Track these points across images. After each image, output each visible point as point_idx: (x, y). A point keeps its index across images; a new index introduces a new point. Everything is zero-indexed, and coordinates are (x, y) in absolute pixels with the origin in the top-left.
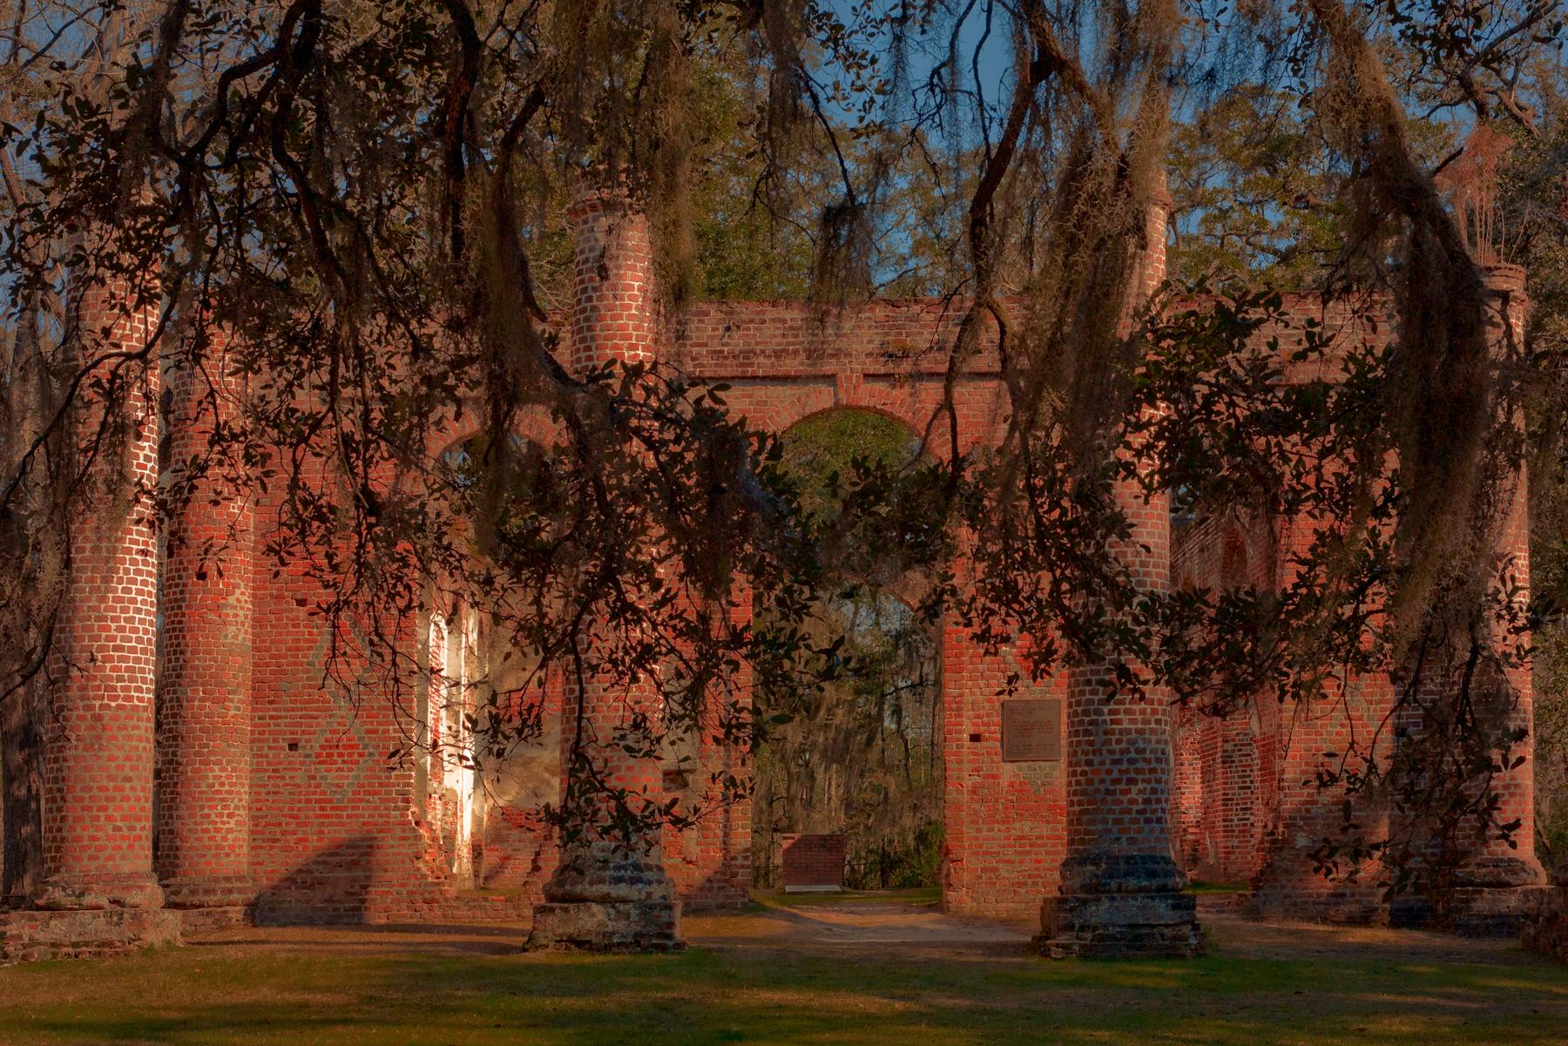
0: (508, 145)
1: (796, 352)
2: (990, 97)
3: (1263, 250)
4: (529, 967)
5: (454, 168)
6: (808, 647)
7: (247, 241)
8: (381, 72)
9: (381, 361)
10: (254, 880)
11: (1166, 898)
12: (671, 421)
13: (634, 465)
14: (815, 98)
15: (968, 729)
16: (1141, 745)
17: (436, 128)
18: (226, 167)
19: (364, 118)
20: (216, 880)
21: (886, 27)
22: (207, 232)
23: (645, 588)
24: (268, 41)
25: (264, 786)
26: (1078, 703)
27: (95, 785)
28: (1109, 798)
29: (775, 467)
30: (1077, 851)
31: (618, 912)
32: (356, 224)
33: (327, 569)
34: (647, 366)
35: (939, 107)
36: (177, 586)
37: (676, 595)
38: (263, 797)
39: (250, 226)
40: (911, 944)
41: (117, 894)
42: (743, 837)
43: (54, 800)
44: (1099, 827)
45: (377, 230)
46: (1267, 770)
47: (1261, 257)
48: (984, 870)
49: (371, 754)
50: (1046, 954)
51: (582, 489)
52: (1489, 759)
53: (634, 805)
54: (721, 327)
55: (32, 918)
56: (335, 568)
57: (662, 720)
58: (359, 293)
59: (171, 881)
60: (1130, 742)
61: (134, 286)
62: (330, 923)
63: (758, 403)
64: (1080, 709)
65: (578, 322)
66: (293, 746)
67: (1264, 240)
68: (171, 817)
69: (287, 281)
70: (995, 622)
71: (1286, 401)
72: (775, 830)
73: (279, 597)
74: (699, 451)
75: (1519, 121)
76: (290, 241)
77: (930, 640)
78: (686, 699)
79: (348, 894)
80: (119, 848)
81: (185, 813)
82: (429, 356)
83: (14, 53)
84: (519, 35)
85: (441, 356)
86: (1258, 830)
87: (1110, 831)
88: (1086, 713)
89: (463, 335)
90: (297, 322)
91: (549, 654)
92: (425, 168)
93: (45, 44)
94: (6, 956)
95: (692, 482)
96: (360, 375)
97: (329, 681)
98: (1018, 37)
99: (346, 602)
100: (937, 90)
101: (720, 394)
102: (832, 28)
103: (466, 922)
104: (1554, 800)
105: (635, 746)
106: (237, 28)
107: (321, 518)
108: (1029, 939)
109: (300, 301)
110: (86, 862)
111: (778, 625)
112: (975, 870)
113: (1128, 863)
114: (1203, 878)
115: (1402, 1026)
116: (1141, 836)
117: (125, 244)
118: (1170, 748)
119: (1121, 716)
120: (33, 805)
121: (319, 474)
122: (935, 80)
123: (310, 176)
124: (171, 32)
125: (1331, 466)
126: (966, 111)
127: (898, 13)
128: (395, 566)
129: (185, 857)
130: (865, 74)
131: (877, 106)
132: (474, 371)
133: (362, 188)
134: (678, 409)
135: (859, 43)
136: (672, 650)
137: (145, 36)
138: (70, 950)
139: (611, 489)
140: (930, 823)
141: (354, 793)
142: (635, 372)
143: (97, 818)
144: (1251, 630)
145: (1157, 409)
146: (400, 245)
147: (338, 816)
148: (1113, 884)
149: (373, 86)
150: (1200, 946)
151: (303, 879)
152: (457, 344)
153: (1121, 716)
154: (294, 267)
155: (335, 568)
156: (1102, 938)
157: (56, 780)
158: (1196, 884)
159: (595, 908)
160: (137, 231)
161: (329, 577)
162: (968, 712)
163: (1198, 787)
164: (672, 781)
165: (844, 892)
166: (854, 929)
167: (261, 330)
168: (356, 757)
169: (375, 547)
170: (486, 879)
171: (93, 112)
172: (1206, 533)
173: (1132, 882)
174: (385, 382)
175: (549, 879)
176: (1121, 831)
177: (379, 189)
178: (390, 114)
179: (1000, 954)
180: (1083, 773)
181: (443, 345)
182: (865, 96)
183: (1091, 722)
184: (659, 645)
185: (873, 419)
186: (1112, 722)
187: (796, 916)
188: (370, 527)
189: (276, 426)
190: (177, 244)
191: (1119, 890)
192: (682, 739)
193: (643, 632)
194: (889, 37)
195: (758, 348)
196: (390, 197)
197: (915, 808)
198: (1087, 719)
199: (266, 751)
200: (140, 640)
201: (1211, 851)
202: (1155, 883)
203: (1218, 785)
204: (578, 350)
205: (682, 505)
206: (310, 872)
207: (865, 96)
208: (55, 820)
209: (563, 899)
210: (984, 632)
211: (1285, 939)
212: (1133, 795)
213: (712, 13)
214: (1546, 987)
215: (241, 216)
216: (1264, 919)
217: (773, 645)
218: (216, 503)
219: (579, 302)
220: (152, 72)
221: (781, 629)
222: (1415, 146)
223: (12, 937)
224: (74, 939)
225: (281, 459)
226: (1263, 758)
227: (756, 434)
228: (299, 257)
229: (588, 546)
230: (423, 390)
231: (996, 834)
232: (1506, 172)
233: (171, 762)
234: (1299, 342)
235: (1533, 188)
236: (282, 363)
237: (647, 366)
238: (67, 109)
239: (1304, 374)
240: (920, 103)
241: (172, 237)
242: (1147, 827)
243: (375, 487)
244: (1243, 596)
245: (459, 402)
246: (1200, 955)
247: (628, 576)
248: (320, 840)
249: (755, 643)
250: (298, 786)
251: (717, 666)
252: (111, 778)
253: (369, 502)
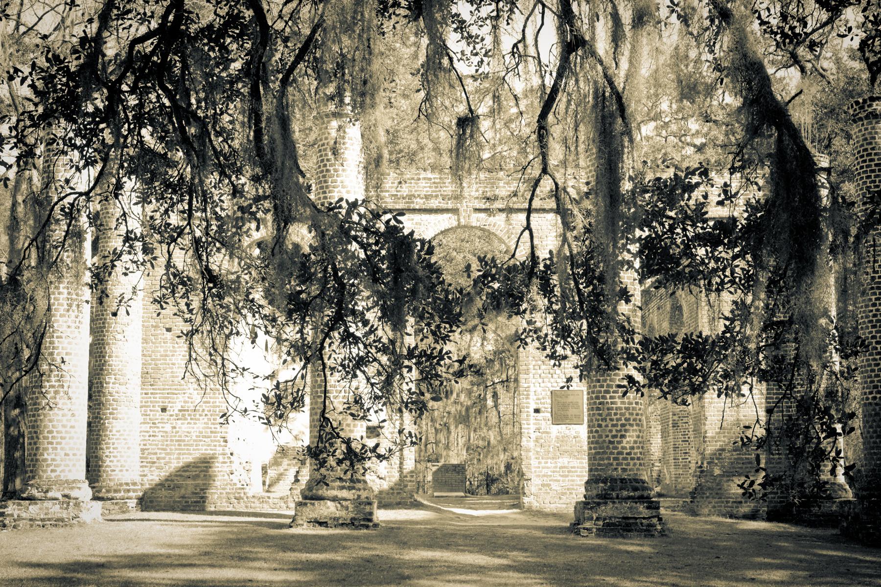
0: (285, 82)
1: (437, 196)
2: (544, 60)
3: (688, 144)
4: (293, 536)
5: (255, 94)
6: (449, 358)
7: (144, 132)
8: (216, 41)
9: (216, 198)
10: (142, 485)
11: (644, 503)
12: (373, 233)
13: (354, 256)
14: (451, 59)
15: (533, 406)
16: (627, 416)
17: (246, 71)
18: (132, 91)
19: (207, 66)
20: (121, 485)
21: (488, 22)
22: (123, 126)
23: (360, 324)
24: (154, 25)
25: (147, 432)
26: (593, 392)
27: (55, 430)
28: (611, 446)
29: (430, 258)
30: (594, 475)
31: (342, 506)
32: (202, 123)
33: (186, 311)
34: (360, 203)
35: (517, 64)
36: (101, 319)
37: (376, 329)
38: (147, 438)
39: (146, 124)
40: (504, 527)
41: (66, 492)
42: (409, 465)
43: (32, 438)
44: (606, 462)
45: (214, 127)
46: (697, 431)
47: (687, 148)
50: (578, 533)
51: (325, 270)
52: (835, 429)
53: (356, 446)
54: (396, 182)
55: (19, 505)
56: (191, 311)
57: (371, 398)
58: (204, 161)
59: (96, 485)
60: (622, 414)
61: (83, 156)
62: (184, 510)
64: (594, 396)
65: (319, 178)
66: (164, 410)
67: (688, 139)
68: (96, 448)
69: (166, 154)
70: (558, 348)
71: (714, 228)
72: (429, 461)
73: (156, 327)
74: (388, 248)
75: (823, 76)
76: (167, 132)
77: (512, 356)
78: (383, 387)
79: (194, 493)
80: (68, 465)
81: (104, 447)
82: (242, 196)
83: (17, 28)
84: (290, 23)
85: (249, 196)
86: (693, 466)
87: (612, 464)
88: (597, 398)
89: (260, 184)
90: (171, 176)
91: (308, 360)
92: (238, 93)
93: (33, 23)
94: (4, 526)
95: (384, 267)
96: (205, 206)
97: (187, 374)
98: (561, 30)
99: (197, 331)
100: (516, 55)
101: (399, 218)
102: (459, 22)
103: (258, 510)
104: (855, 450)
105: (356, 413)
106: (139, 17)
107: (184, 284)
108: (568, 525)
109: (173, 164)
110: (49, 473)
111: (432, 345)
112: (538, 485)
113: (622, 482)
114: (663, 492)
115: (778, 575)
116: (629, 467)
117: (78, 132)
118: (644, 418)
120: (21, 440)
121: (182, 259)
122: (515, 50)
123: (178, 97)
124: (104, 18)
125: (740, 263)
126: (532, 65)
127: (494, 14)
128: (224, 311)
129: (104, 471)
130: (478, 47)
131: (485, 63)
132: (267, 204)
133: (206, 103)
134: (377, 226)
135: (474, 30)
136: (375, 360)
137: (90, 21)
138: (40, 523)
139: (341, 269)
140: (513, 458)
141: (197, 436)
142: (354, 205)
143: (56, 449)
144: (700, 357)
145: (644, 231)
146: (228, 136)
147: (188, 449)
148: (614, 494)
149: (212, 49)
150: (663, 530)
151: (169, 484)
152: (257, 189)
153: (617, 400)
154: (170, 146)
155: (191, 311)
156: (608, 525)
157: (33, 427)
158: (660, 495)
159: (329, 503)
160: (85, 126)
161: (187, 316)
162: (532, 396)
163: (659, 441)
164: (371, 432)
165: (466, 497)
166: (472, 517)
167: (151, 181)
168: (198, 416)
169: (213, 301)
170: (269, 486)
171: (62, 62)
172: (661, 299)
173: (625, 493)
174: (218, 209)
175: (303, 487)
176: (618, 464)
177: (214, 104)
178: (221, 64)
179: (552, 533)
180: (597, 431)
181: (250, 189)
182: (478, 59)
183: (600, 403)
184: (368, 357)
185: (479, 233)
186: (612, 403)
187: (440, 509)
188: (210, 289)
189: (160, 233)
190: (107, 132)
191: (617, 498)
192: (381, 410)
193: (359, 349)
194: (490, 27)
195: (416, 194)
196: (221, 110)
197: (505, 450)
199: (149, 412)
201: (668, 476)
202: (637, 494)
203: (671, 439)
204: (319, 193)
205: (379, 279)
206: (172, 481)
207: (478, 59)
208: (32, 449)
209: (312, 498)
210: (553, 353)
211: (708, 527)
212: (624, 444)
213: (394, 13)
214: (854, 556)
215: (140, 120)
216: (697, 515)
217: (430, 357)
218: (126, 274)
219: (319, 167)
220: (94, 40)
221: (435, 348)
222: (775, 88)
223: (8, 515)
224: (42, 517)
225: (161, 251)
226: (695, 424)
227: (419, 240)
228: (172, 141)
229: (328, 301)
230: (239, 214)
231: (549, 465)
232: (816, 104)
233: (97, 418)
234: (719, 195)
235: (832, 112)
236: (163, 198)
237: (360, 203)
238: (48, 60)
239: (722, 212)
240: (507, 63)
241: (103, 129)
242: (632, 463)
243: (214, 267)
244: (694, 337)
245: (258, 221)
246: (662, 535)
247: (350, 319)
248: (178, 463)
249: (420, 356)
250: (166, 432)
251: (400, 368)
252: (64, 426)
253: (210, 276)
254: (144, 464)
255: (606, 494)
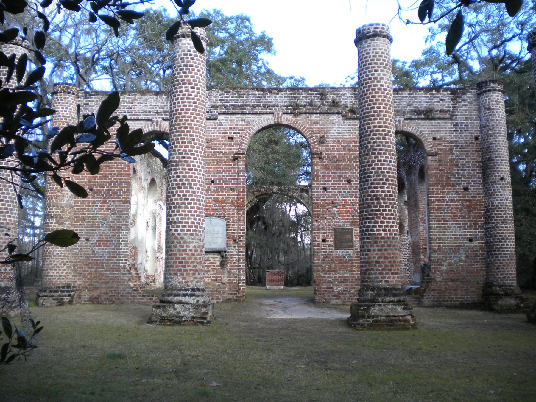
11: (401, 305)
20: (59, 287)
28: (377, 265)
38: (77, 258)
44: (374, 276)
48: (328, 288)
49: (114, 244)
63: (247, 122)
87: (378, 278)
119: (381, 232)
159: (176, 306)
168: (108, 245)
173: (388, 299)
191: (382, 302)
198: (368, 233)
200: (11, 198)
202: (396, 299)
231: (331, 275)
242: (392, 276)
254: (75, 274)
255: (375, 299)
